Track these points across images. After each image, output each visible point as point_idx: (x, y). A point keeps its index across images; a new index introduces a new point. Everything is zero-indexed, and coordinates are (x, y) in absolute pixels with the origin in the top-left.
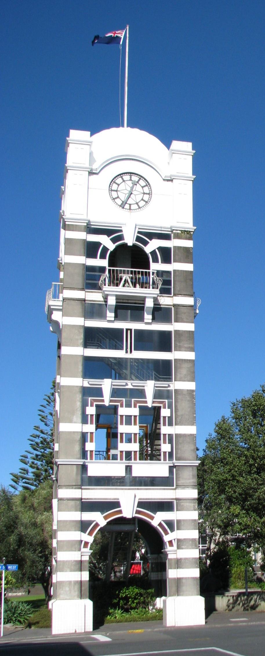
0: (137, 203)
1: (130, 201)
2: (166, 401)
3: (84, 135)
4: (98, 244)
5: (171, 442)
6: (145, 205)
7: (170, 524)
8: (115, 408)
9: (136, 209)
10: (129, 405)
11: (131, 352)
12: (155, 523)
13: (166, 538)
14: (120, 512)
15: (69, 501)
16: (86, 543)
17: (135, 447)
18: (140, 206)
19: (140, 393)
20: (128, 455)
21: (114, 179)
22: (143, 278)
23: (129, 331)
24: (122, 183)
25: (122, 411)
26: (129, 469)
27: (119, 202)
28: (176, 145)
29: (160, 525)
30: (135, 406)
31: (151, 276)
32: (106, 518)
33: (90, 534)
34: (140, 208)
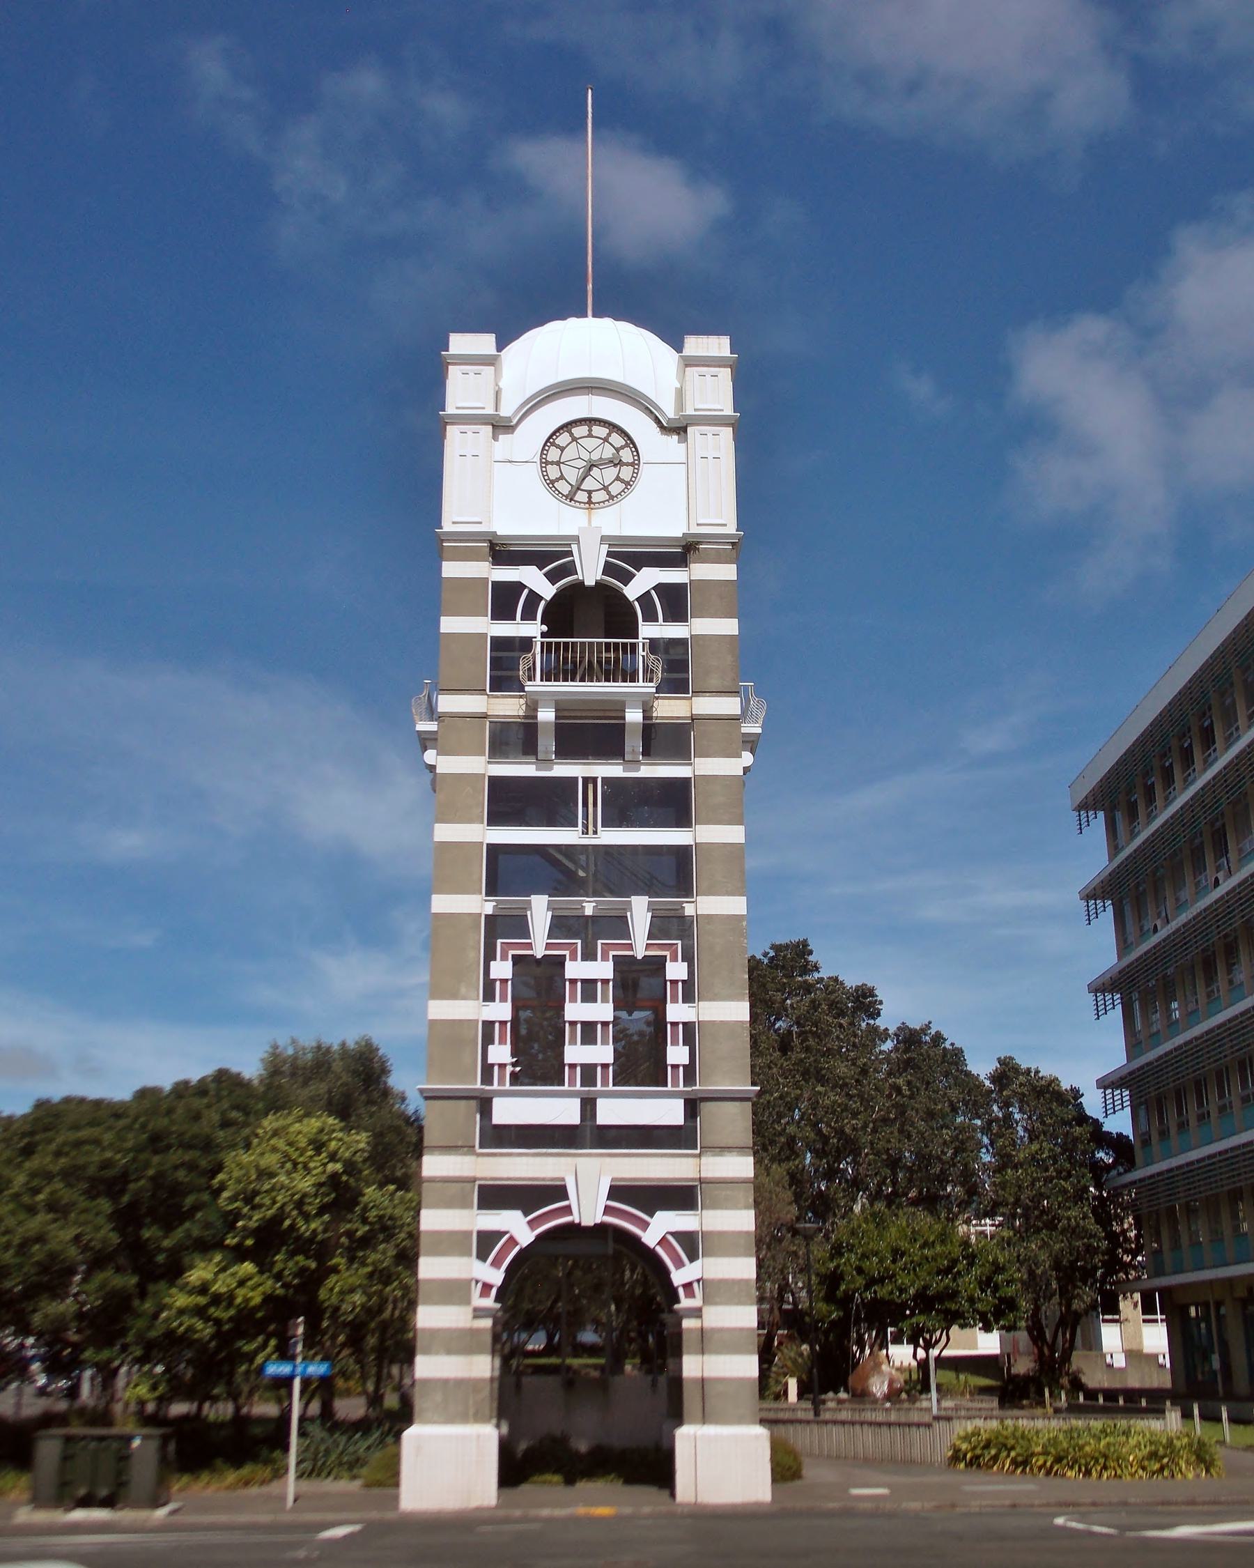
0: (605, 488)
1: (589, 484)
2: (679, 942)
3: (484, 343)
4: (520, 586)
5: (689, 1040)
6: (623, 491)
7: (690, 1244)
8: (559, 962)
9: (603, 502)
10: (589, 955)
11: (595, 832)
12: (650, 1238)
13: (678, 1277)
14: (567, 1210)
15: (446, 1184)
16: (487, 1287)
17: (603, 1053)
18: (614, 494)
19: (618, 925)
20: (589, 1072)
21: (550, 437)
22: (625, 660)
23: (591, 787)
24: (570, 443)
25: (575, 969)
26: (588, 1106)
27: (564, 488)
28: (695, 345)
29: (663, 1241)
30: (605, 958)
31: (641, 652)
32: (532, 1224)
33: (496, 1264)
34: (612, 497)
